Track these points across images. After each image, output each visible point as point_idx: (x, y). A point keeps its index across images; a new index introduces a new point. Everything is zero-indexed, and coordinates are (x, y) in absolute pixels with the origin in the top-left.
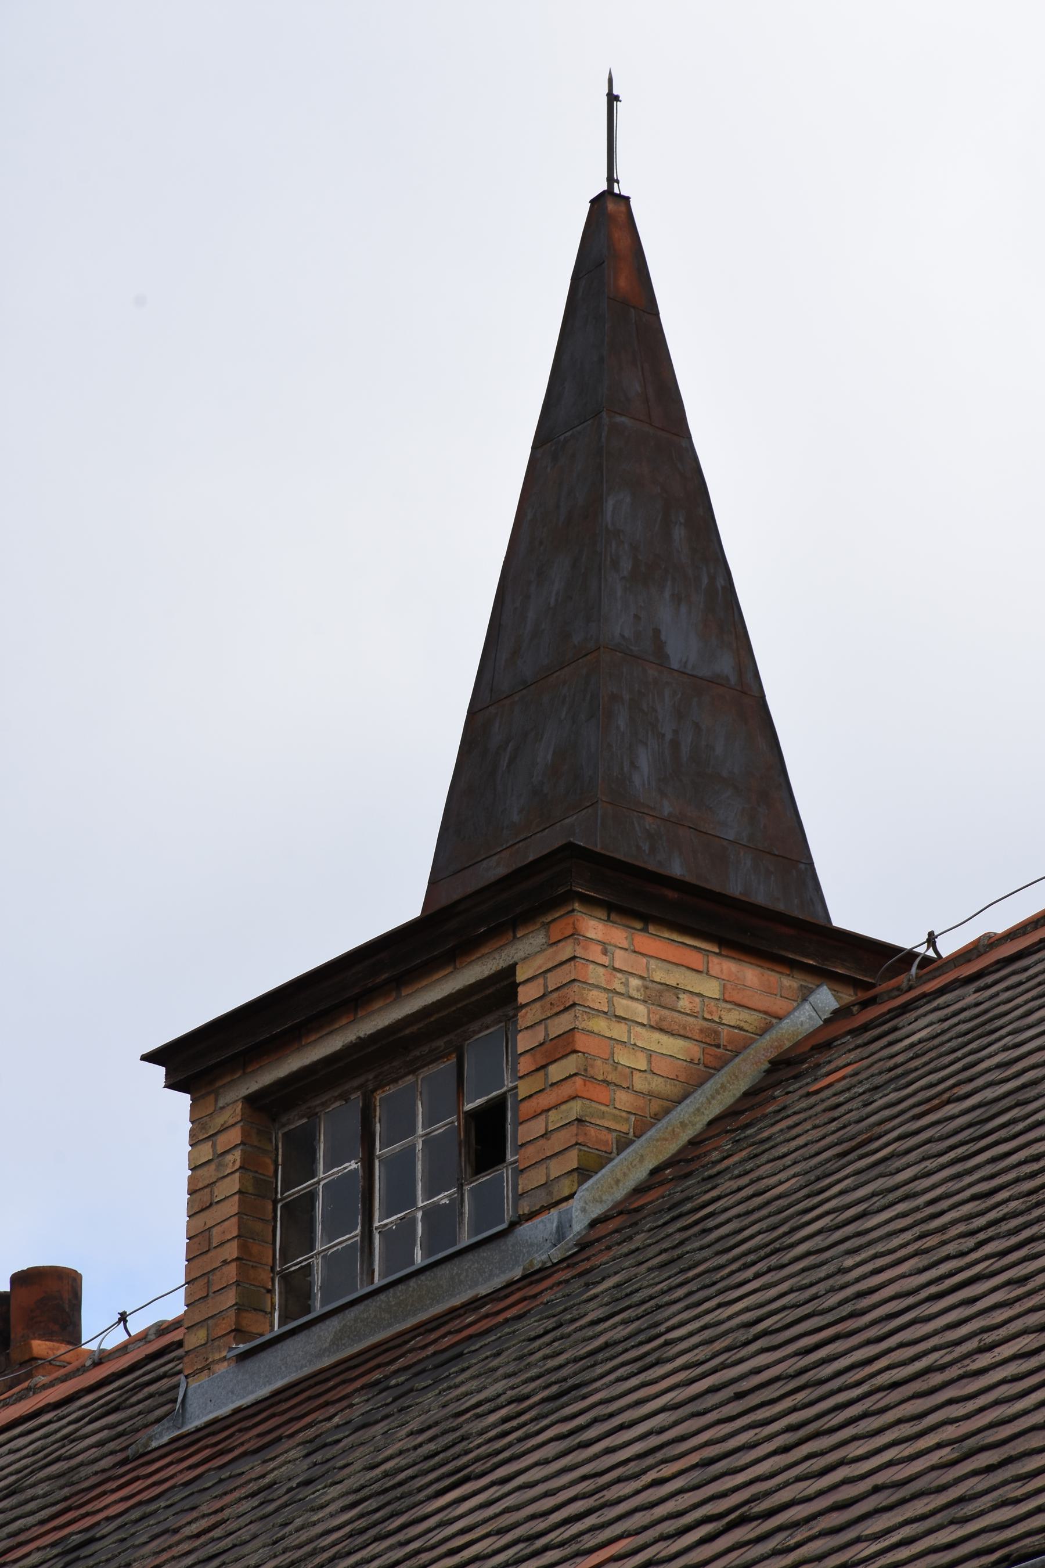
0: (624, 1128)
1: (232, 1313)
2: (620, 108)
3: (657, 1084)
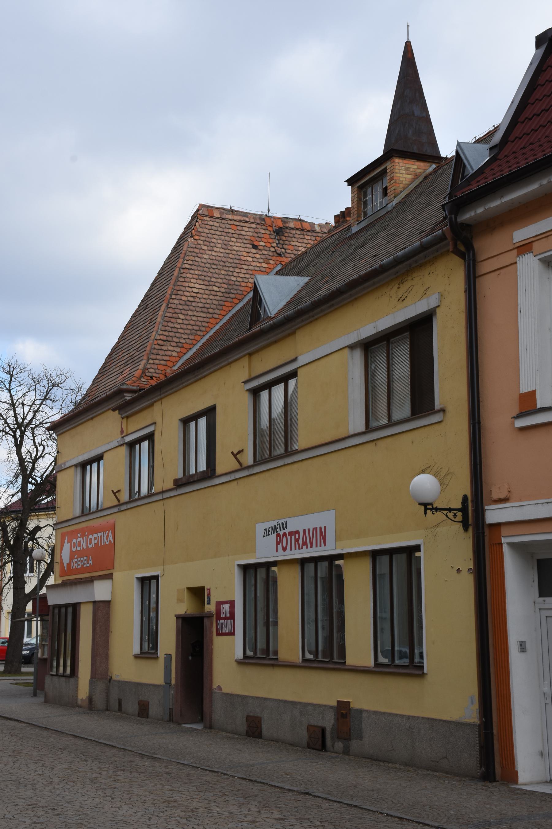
0: (401, 190)
1: (356, 218)
2: (409, 27)
3: (407, 182)
